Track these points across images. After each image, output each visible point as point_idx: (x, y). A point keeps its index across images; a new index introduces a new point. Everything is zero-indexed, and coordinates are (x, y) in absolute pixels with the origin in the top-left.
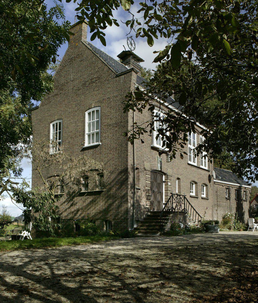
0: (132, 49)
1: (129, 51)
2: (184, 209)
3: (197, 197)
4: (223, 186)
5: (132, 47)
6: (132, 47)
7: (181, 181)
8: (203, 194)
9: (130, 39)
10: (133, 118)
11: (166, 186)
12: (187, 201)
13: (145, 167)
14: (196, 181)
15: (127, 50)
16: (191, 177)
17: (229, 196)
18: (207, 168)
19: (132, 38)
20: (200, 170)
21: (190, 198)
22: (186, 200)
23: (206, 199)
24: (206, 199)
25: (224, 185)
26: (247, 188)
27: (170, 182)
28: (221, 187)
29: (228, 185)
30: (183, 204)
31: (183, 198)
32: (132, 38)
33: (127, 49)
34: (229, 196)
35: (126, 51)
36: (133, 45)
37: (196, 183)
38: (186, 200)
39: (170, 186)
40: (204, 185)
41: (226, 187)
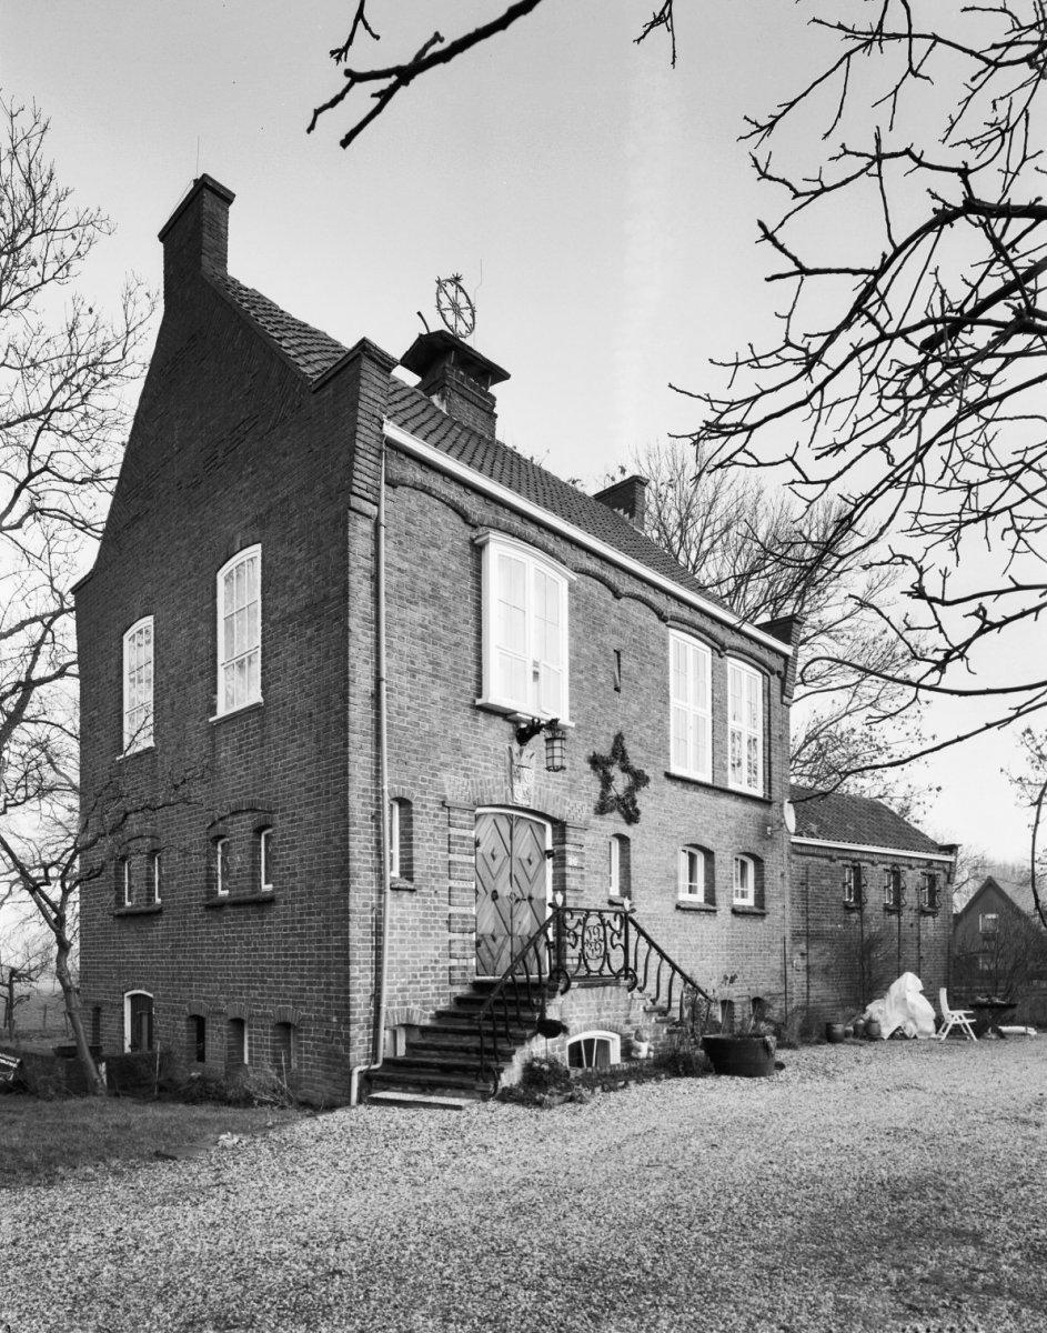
0: (462, 328)
1: (441, 333)
2: (626, 967)
3: (712, 908)
4: (831, 859)
5: (460, 323)
6: (460, 323)
7: (634, 846)
8: (744, 895)
9: (451, 289)
10: (375, 578)
11: (560, 870)
12: (641, 932)
13: (448, 793)
14: (708, 843)
15: (433, 329)
16: (681, 829)
17: (897, 901)
18: (759, 792)
19: (461, 283)
20: (725, 801)
21: (679, 915)
22: (631, 927)
23: (755, 914)
24: (755, 914)
25: (876, 858)
26: (935, 865)
27: (576, 853)
28: (825, 862)
29: (858, 856)
30: (620, 951)
31: (617, 925)
32: (461, 283)
33: (436, 325)
34: (897, 901)
35: (430, 335)
36: (446, 304)
37: (709, 854)
38: (631, 927)
39: (579, 872)
40: (745, 858)
41: (845, 862)
